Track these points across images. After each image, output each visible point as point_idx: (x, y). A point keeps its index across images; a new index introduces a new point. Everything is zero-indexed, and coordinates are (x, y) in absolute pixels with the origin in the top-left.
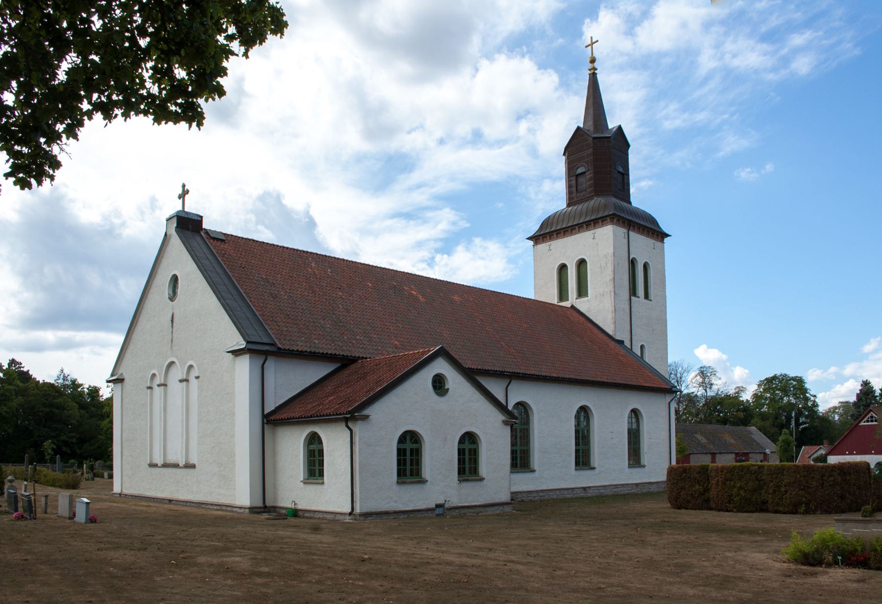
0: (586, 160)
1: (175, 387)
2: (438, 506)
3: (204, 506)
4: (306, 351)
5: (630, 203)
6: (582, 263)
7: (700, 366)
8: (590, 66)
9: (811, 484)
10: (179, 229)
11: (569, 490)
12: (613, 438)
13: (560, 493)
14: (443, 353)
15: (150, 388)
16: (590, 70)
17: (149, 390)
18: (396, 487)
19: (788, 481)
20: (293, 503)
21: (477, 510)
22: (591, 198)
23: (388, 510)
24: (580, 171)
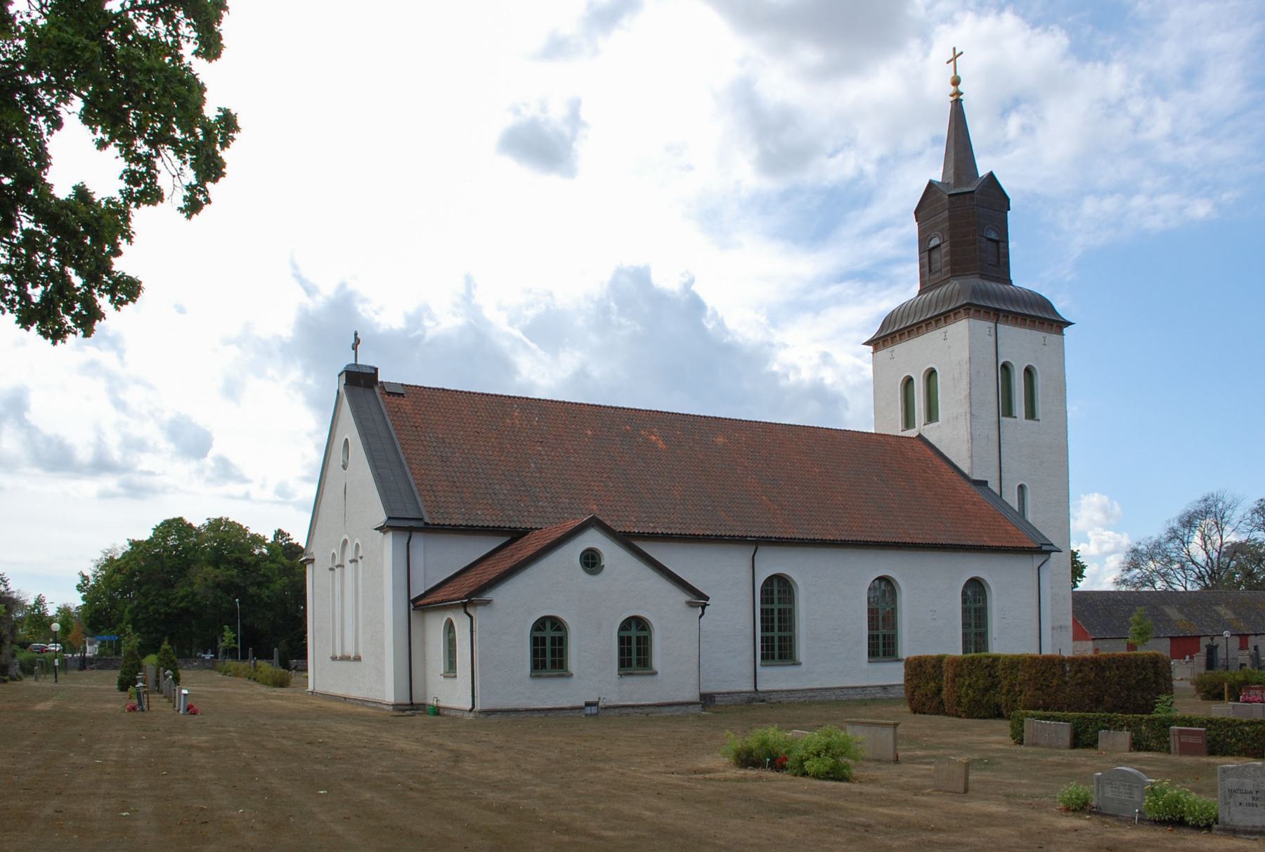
0: (940, 227)
1: (349, 567)
2: (588, 704)
3: (366, 704)
4: (461, 525)
5: (1010, 282)
6: (931, 374)
7: (1260, 498)
8: (952, 89)
9: (1052, 683)
10: (348, 387)
11: (857, 689)
12: (934, 619)
13: (841, 693)
14: (595, 523)
15: (332, 569)
16: (952, 96)
17: (331, 572)
18: (530, 682)
19: (1022, 677)
20: (435, 699)
21: (647, 710)
22: (946, 281)
23: (518, 707)
24: (934, 243)
